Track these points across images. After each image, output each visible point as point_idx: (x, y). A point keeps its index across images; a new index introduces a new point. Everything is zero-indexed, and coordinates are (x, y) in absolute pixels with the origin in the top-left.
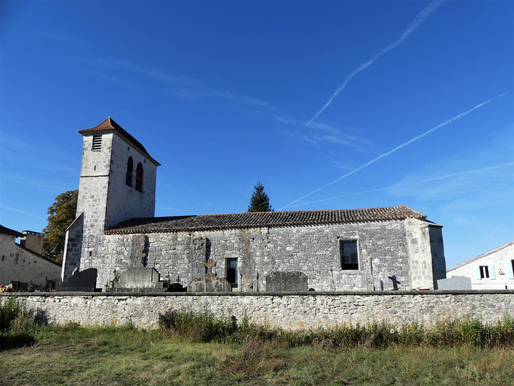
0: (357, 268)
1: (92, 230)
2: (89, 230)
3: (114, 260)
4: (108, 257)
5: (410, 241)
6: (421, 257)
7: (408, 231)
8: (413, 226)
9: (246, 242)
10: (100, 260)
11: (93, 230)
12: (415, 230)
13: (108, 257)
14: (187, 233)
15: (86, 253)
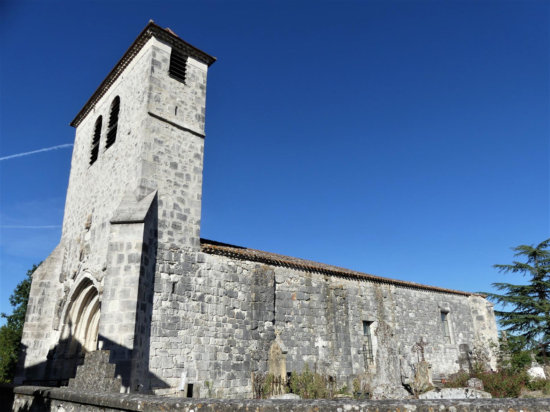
0: (188, 396)
1: (177, 237)
2: (170, 233)
3: (221, 306)
4: (210, 300)
5: (475, 318)
6: (488, 334)
7: (473, 308)
8: (478, 304)
9: (379, 299)
10: (195, 303)
11: (180, 237)
12: (481, 308)
13: (210, 300)
14: (323, 276)
15: (165, 286)
